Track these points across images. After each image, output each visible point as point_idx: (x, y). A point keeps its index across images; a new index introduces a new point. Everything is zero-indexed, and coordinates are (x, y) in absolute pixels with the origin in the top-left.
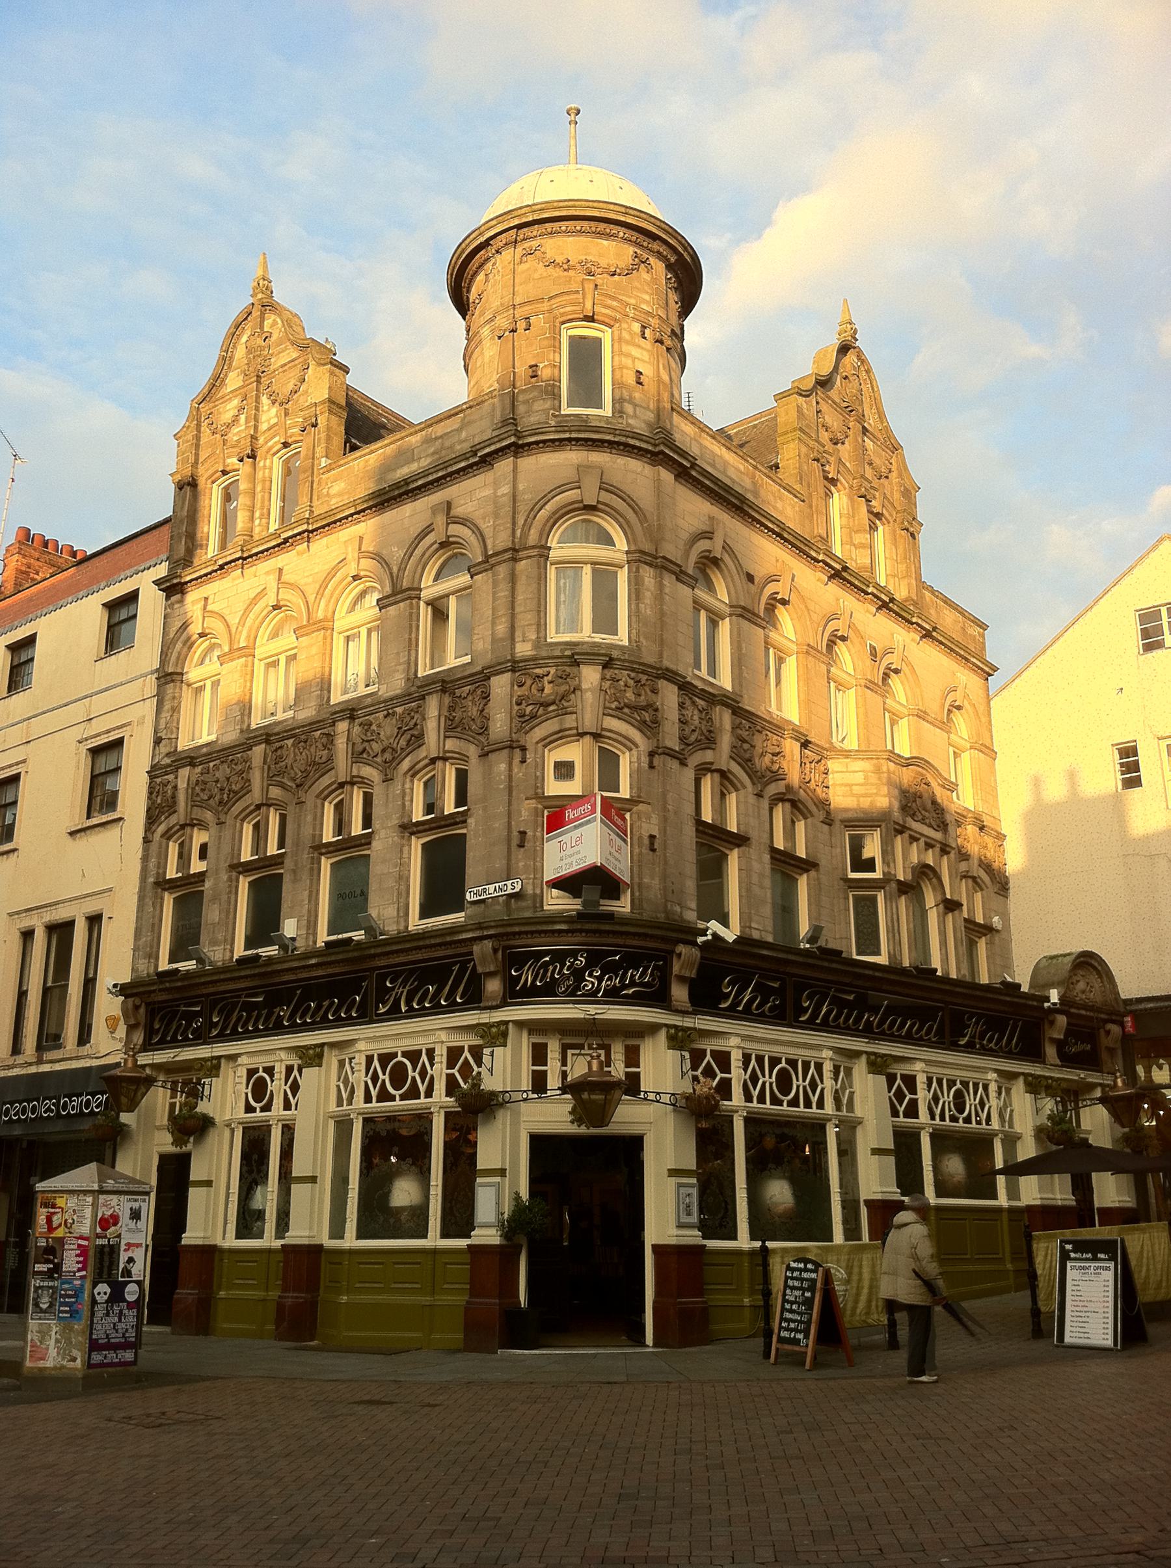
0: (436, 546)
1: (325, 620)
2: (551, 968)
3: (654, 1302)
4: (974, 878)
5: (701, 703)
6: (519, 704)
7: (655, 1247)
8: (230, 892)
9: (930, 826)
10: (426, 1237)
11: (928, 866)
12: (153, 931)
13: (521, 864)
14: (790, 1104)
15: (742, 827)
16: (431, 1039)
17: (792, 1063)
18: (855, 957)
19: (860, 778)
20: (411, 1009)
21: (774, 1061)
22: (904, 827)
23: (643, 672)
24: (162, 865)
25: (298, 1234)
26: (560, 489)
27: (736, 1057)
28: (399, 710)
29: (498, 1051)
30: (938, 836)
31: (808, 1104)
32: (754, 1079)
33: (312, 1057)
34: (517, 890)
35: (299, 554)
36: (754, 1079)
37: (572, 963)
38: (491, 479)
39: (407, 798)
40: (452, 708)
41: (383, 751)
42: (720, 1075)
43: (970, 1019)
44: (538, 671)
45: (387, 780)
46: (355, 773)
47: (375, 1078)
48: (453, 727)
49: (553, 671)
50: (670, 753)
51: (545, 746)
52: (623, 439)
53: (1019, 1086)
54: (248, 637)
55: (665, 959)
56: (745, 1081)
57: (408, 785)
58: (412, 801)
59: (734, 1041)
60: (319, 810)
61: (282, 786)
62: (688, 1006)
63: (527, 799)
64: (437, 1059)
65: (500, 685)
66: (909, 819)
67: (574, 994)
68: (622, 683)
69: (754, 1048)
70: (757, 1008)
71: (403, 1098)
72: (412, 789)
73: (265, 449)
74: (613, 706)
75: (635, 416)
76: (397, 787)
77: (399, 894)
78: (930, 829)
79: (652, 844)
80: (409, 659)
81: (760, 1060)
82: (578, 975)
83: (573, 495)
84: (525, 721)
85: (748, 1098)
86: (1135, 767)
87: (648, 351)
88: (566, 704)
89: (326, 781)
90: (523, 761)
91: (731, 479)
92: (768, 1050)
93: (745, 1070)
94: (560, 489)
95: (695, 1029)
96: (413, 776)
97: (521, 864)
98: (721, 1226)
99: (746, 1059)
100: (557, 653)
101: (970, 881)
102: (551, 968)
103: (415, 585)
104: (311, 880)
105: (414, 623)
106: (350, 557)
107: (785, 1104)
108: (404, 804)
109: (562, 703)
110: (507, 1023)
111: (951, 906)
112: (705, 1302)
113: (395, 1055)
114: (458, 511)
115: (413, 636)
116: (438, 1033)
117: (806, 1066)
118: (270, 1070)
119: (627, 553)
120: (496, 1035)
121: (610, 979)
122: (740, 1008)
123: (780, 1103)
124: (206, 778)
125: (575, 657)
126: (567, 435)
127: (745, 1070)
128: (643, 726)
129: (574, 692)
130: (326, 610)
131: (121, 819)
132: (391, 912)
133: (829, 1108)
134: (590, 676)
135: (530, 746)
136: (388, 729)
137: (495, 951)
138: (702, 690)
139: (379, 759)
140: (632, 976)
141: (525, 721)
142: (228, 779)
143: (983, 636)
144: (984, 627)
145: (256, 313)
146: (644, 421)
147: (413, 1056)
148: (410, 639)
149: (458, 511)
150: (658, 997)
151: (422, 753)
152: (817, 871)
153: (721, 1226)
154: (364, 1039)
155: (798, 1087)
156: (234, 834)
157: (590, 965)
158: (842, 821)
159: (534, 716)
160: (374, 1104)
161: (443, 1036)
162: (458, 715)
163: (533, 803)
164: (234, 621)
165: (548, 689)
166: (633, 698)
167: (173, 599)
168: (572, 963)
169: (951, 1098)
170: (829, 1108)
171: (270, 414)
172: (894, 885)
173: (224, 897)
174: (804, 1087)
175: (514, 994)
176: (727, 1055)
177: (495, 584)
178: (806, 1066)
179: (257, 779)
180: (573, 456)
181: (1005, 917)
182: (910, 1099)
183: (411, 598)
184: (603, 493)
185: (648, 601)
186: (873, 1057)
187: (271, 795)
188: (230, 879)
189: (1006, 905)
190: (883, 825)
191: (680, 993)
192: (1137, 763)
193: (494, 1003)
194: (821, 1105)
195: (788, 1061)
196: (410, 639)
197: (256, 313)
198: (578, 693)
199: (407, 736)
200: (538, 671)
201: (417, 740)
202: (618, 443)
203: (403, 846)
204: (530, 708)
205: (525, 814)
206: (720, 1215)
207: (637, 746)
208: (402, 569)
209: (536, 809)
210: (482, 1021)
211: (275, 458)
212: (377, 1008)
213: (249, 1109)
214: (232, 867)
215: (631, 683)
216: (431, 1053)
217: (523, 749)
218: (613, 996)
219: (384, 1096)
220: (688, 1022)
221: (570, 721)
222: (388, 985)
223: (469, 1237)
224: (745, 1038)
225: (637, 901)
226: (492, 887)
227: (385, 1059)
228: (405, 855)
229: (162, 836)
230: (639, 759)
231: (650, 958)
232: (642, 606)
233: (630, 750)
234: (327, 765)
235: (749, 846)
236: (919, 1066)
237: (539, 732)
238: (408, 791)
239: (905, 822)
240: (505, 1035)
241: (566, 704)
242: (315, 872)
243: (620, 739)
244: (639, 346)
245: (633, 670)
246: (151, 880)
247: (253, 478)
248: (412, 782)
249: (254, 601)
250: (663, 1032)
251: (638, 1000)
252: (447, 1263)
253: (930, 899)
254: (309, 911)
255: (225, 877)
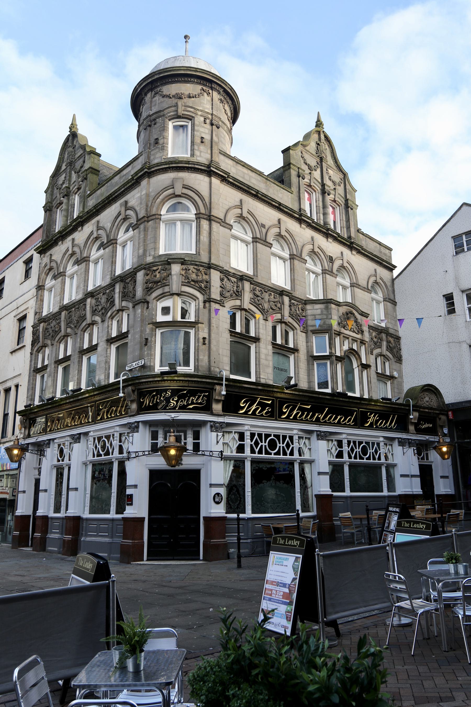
0: (122, 220)
1: (87, 257)
2: (156, 397)
3: (204, 541)
4: (384, 356)
5: (233, 279)
6: (146, 283)
7: (204, 517)
8: (55, 373)
9: (354, 332)
10: (109, 513)
11: (354, 350)
12: (32, 390)
13: (146, 353)
14: (367, 459)
15: (257, 334)
16: (112, 430)
17: (367, 443)
18: (317, 390)
19: (319, 312)
20: (377, 427)
21: (360, 443)
22: (340, 332)
23: (201, 266)
24: (36, 363)
25: (72, 512)
26: (166, 189)
27: (345, 442)
28: (108, 291)
29: (135, 434)
30: (359, 336)
31: (374, 459)
32: (352, 450)
33: (76, 438)
34: (143, 364)
35: (80, 231)
36: (352, 450)
37: (165, 395)
38: (140, 190)
39: (110, 328)
40: (124, 288)
41: (102, 309)
42: (339, 449)
43: (370, 415)
44: (155, 268)
45: (103, 321)
46: (93, 320)
47: (96, 447)
48: (125, 296)
49: (160, 267)
50: (216, 302)
51: (157, 301)
52: (193, 166)
53: (314, 437)
54: (63, 268)
55: (209, 392)
56: (348, 451)
57: (110, 323)
58: (112, 329)
59: (246, 428)
60: (82, 336)
61: (71, 327)
62: (221, 413)
63: (149, 324)
64: (115, 439)
65: (140, 276)
66: (342, 329)
67: (165, 409)
68: (190, 271)
69: (352, 438)
70: (259, 413)
71: (275, 454)
72: (112, 324)
73: (72, 192)
74: (186, 281)
75: (200, 156)
76: (106, 324)
77: (106, 369)
78: (354, 333)
79: (204, 341)
80: (112, 269)
81: (354, 442)
82: (168, 400)
83: (170, 191)
84: (148, 290)
85: (350, 457)
86: (453, 304)
87: (208, 129)
88: (165, 282)
89: (84, 324)
90: (147, 308)
91: (253, 184)
92: (264, 431)
93: (349, 447)
94: (166, 189)
95: (224, 422)
96: (112, 319)
97: (146, 353)
98: (237, 508)
99: (349, 442)
100: (163, 259)
101: (382, 357)
102: (156, 397)
103: (115, 238)
104: (79, 366)
105: (114, 254)
106: (94, 230)
107: (365, 459)
108: (108, 331)
109: (163, 282)
110: (138, 422)
111: (366, 367)
112: (226, 541)
113: (270, 435)
114: (130, 204)
115: (114, 259)
116: (116, 427)
117: (373, 444)
118: (64, 444)
119: (196, 214)
120: (134, 428)
121: (182, 401)
122: (250, 413)
123: (363, 459)
124: (49, 327)
125: (168, 261)
126: (168, 166)
127: (349, 447)
128: (200, 290)
129: (168, 276)
130: (87, 253)
131: (24, 346)
132: (102, 377)
133: (383, 460)
134: (176, 269)
135: (151, 301)
136: (103, 299)
137: (133, 391)
138: (234, 273)
139: (101, 313)
140: (192, 400)
141: (148, 290)
142: (55, 326)
143: (390, 253)
144: (390, 250)
145: (70, 138)
146: (205, 158)
147: (108, 437)
148: (112, 261)
149: (130, 204)
150: (207, 409)
151: (114, 309)
152: (298, 353)
153: (237, 508)
154: (93, 431)
155: (370, 452)
156: (56, 349)
157: (173, 396)
158: (311, 331)
159: (152, 288)
160: (96, 458)
161: (117, 429)
162: (126, 290)
163: (151, 326)
164: (59, 262)
165: (158, 275)
166: (196, 277)
167: (42, 256)
168: (165, 395)
169: (360, 450)
170: (383, 460)
171: (74, 176)
172: (334, 358)
173: (53, 375)
174: (373, 452)
175: (142, 410)
176: (341, 441)
177: (139, 233)
178: (373, 444)
179: (63, 325)
180: (171, 175)
181: (400, 372)
182: (339, 450)
183: (113, 244)
184: (184, 189)
185: (205, 235)
186: (400, 440)
187: (68, 332)
188: (55, 367)
189: (400, 367)
190: (329, 332)
191: (217, 407)
192: (453, 303)
193: (133, 414)
194: (379, 459)
195: (366, 443)
196: (112, 261)
197: (70, 138)
198: (170, 276)
199: (110, 302)
200: (155, 268)
201: (112, 304)
202: (191, 168)
203: (107, 349)
204: (151, 284)
205: (148, 331)
206: (237, 503)
207: (198, 299)
208: (111, 232)
209: (153, 328)
210: (129, 422)
211: (77, 196)
212: (97, 418)
213: (59, 461)
214: (56, 362)
215: (194, 271)
216: (291, 438)
217: (148, 303)
218: (183, 408)
219: (99, 455)
220: (221, 419)
221: (167, 289)
222: (101, 408)
223: (123, 514)
224: (348, 434)
225: (196, 367)
226: (134, 364)
227: (99, 439)
228: (108, 352)
229: (36, 352)
230: (199, 304)
231: (202, 392)
232: (201, 237)
233: (195, 300)
234: (83, 318)
235: (259, 342)
236: (344, 436)
237: (154, 295)
238: (110, 325)
239: (340, 330)
240: (137, 427)
241: (165, 282)
242: (80, 362)
243: (190, 295)
244: (203, 127)
245: (196, 265)
246: (32, 369)
247: (68, 204)
248: (112, 321)
249: (65, 254)
250: (397, 440)
251: (195, 410)
252: (117, 525)
253: (355, 364)
254: (78, 379)
255: (53, 367)
